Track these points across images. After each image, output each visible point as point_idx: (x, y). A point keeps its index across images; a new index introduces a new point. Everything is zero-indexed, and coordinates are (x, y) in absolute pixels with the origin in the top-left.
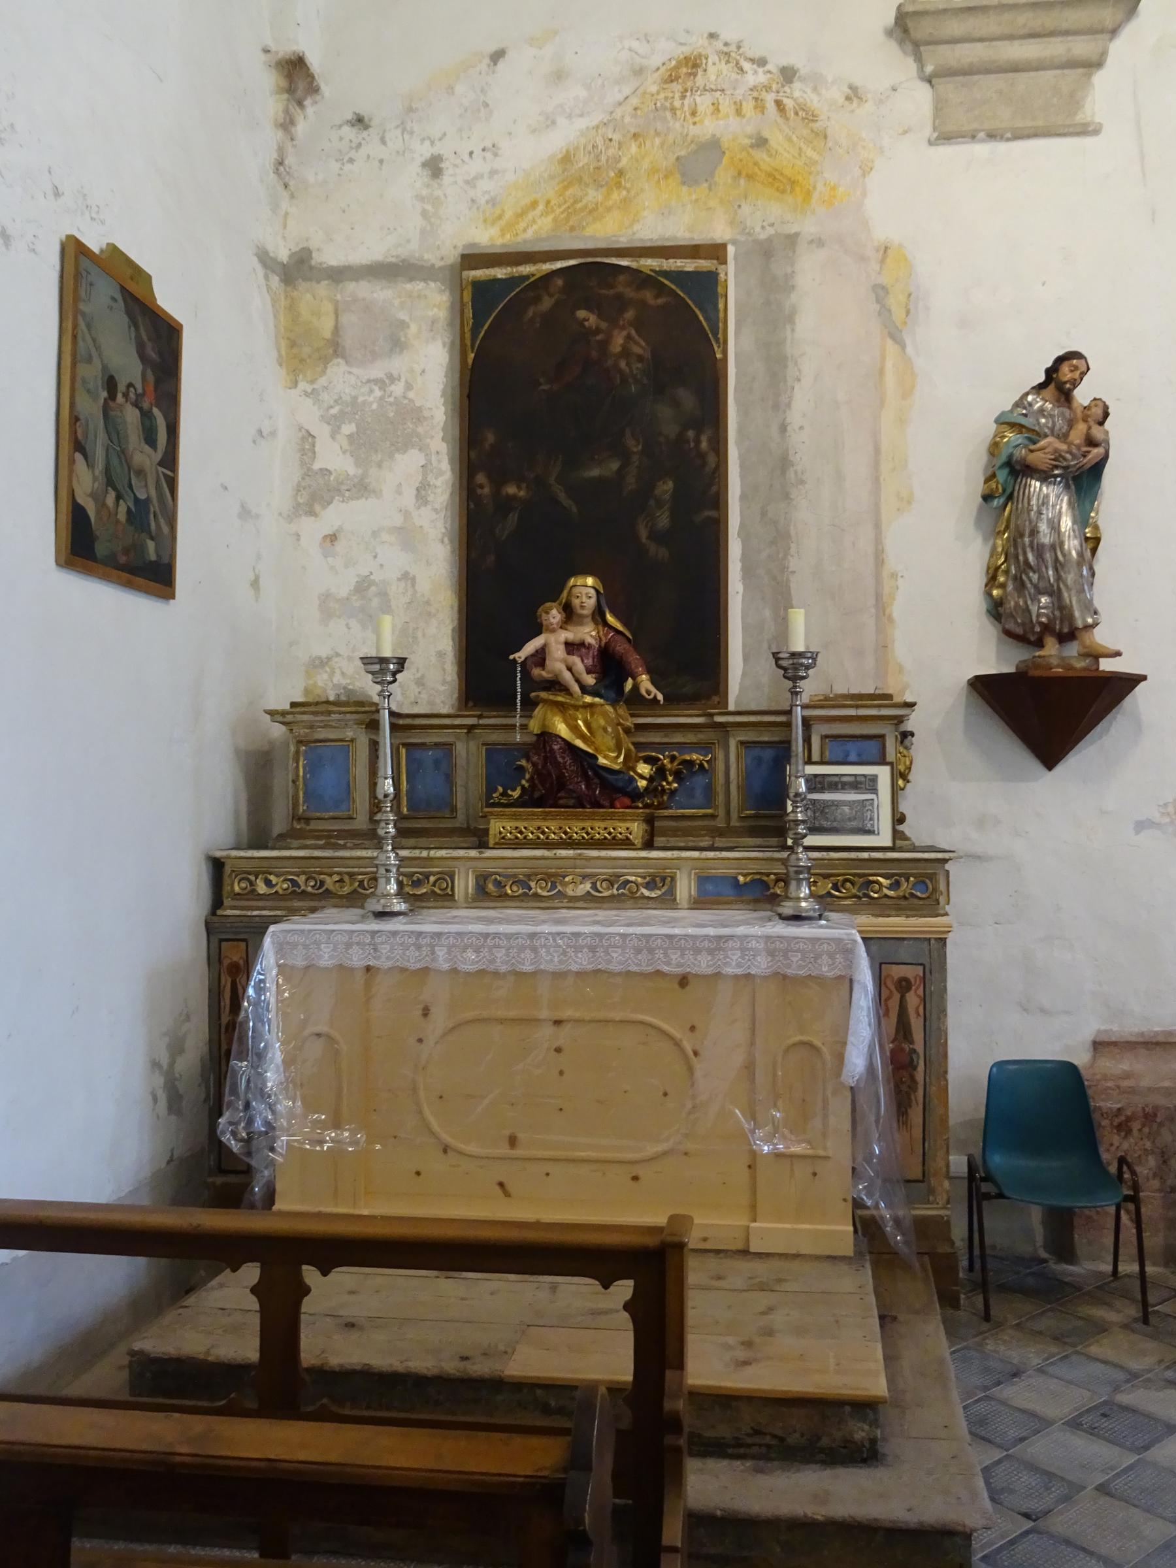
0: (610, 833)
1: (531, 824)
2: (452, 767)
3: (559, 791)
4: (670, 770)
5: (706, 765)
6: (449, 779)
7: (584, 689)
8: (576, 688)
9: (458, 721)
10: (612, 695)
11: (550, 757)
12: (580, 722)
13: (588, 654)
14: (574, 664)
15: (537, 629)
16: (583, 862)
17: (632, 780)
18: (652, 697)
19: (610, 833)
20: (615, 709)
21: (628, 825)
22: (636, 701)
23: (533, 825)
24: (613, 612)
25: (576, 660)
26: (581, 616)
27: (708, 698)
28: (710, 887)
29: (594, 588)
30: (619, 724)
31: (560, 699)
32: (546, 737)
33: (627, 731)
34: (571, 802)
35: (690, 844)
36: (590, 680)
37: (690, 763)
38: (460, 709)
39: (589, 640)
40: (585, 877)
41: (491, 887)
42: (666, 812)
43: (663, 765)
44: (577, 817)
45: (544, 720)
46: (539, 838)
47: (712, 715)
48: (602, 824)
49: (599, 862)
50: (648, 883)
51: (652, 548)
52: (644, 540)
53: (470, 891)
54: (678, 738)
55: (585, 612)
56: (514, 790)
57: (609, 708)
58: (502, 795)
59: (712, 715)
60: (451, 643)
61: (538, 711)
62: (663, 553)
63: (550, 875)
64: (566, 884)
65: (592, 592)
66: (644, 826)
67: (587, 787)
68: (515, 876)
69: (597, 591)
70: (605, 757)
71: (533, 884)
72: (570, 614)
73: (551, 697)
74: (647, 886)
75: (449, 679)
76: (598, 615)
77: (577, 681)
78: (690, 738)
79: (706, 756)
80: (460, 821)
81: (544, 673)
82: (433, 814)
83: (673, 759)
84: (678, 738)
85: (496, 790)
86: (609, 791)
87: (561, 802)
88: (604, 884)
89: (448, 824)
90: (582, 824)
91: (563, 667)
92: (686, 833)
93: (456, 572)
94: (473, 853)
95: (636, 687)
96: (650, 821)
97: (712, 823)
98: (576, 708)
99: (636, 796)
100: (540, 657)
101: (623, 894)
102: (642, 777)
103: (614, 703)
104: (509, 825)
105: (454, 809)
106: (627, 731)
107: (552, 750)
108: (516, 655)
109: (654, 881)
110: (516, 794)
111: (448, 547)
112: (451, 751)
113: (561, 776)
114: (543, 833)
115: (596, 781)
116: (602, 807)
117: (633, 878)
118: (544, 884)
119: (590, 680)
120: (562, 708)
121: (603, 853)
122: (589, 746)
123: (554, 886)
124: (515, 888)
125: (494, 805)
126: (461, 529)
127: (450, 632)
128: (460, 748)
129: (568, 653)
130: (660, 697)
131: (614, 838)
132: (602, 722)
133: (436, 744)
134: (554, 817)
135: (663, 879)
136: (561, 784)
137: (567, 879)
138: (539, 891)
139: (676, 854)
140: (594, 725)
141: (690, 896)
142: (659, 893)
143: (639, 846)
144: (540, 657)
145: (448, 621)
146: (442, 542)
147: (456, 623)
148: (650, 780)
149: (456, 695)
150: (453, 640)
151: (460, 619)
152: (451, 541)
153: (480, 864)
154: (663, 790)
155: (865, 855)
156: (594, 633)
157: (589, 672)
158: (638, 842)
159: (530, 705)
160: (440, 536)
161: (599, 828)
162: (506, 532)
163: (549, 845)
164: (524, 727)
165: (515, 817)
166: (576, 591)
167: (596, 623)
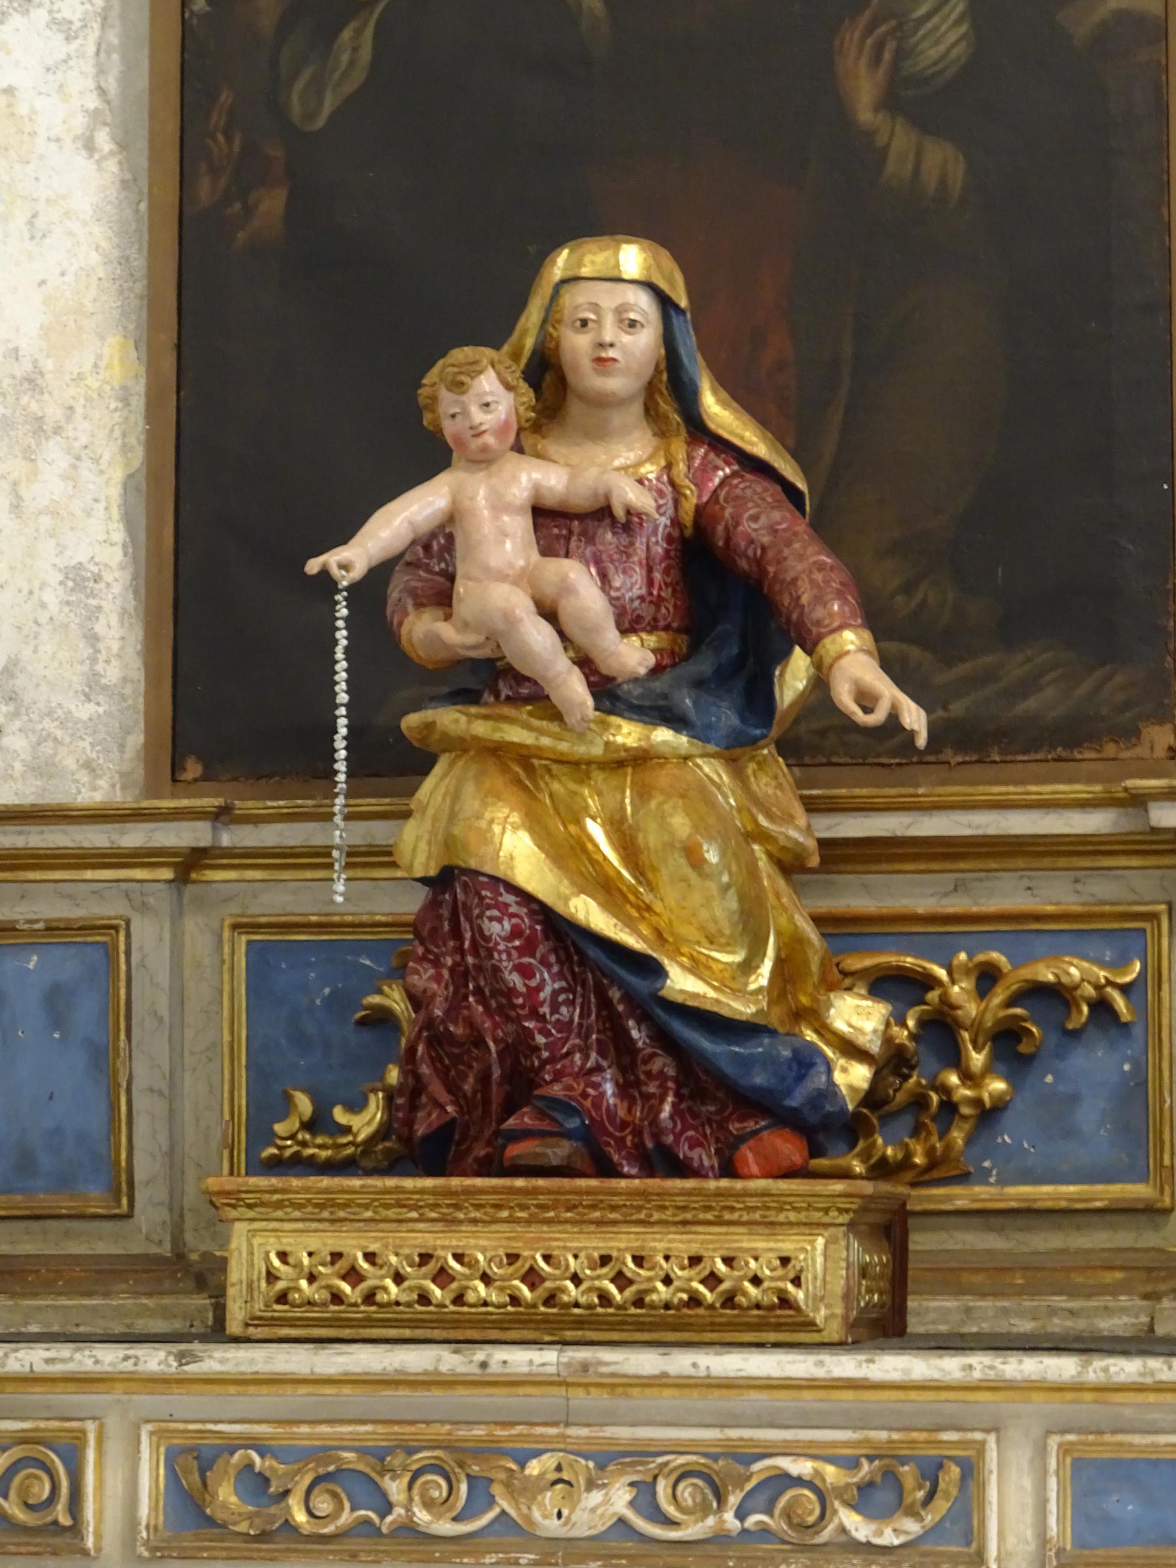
0: (712, 1280)
1: (403, 1235)
2: (118, 1016)
3: (510, 1108)
4: (976, 1027)
5: (1120, 1002)
6: (105, 1062)
7: (608, 693)
8: (574, 689)
9: (134, 837)
10: (727, 717)
11: (473, 975)
12: (595, 830)
13: (626, 552)
14: (567, 588)
15: (429, 455)
16: (600, 1399)
17: (805, 1061)
18: (878, 717)
19: (712, 1280)
20: (738, 774)
21: (787, 1245)
22: (825, 745)
23: (399, 1245)
24: (739, 392)
25: (582, 587)
26: (603, 402)
27: (1129, 734)
28: (1125, 1507)
29: (649, 285)
30: (758, 835)
31: (516, 735)
32: (457, 888)
33: (790, 865)
34: (559, 1151)
35: (1058, 1325)
36: (633, 655)
37: (1055, 996)
38: (151, 791)
39: (631, 495)
40: (607, 1460)
41: (227, 1495)
42: (961, 1197)
43: (946, 1002)
44: (582, 1215)
45: (453, 817)
46: (424, 1299)
47: (1138, 801)
48: (682, 1244)
49: (667, 1399)
50: (866, 1488)
51: (900, 141)
52: (865, 111)
53: (144, 1511)
54: (1006, 893)
55: (614, 384)
56: (356, 1106)
57: (711, 769)
58: (309, 1126)
59: (1138, 801)
60: (119, 535)
61: (432, 789)
62: (941, 163)
63: (463, 1452)
64: (530, 1490)
65: (643, 302)
66: (856, 1251)
67: (623, 1090)
68: (323, 1453)
69: (664, 302)
70: (697, 967)
71: (395, 1488)
72: (552, 394)
73: (481, 729)
74: (863, 1498)
75: (112, 673)
76: (669, 395)
77: (584, 662)
78: (1054, 893)
79: (1121, 963)
80: (147, 1229)
81: (448, 632)
82: (45, 1201)
83: (987, 978)
84: (1006, 893)
85: (286, 1107)
86: (714, 1102)
87: (515, 1150)
88: (686, 1491)
89: (102, 1243)
90: (596, 1244)
91: (521, 604)
92: (1041, 1277)
93: (139, 262)
94: (155, 1360)
95: (820, 683)
96: (889, 1229)
97: (1150, 1239)
98: (580, 768)
99: (825, 1130)
100: (435, 561)
101: (764, 1532)
102: (851, 1050)
103: (734, 750)
104: (308, 1243)
105: (122, 1185)
106: (790, 865)
107: (480, 936)
108: (332, 559)
109: (891, 1477)
110: (365, 1122)
111: (112, 166)
112: (109, 952)
113: (518, 1049)
114: (442, 1276)
115: (662, 1063)
116: (682, 1169)
117: (802, 1467)
118: (439, 1491)
119: (633, 655)
120: (522, 769)
121: (682, 1362)
122: (629, 923)
123: (480, 1489)
124: (323, 1505)
125: (276, 1166)
126: (155, 88)
127: (115, 492)
128: (148, 938)
129: (547, 551)
130: (914, 718)
131: (729, 1300)
132: (681, 824)
133: (52, 928)
134: (491, 1212)
135: (931, 1472)
136: (522, 1084)
137: (534, 1468)
138: (422, 1516)
139: (981, 1364)
140: (650, 838)
141: (1043, 1539)
142: (912, 1527)
143: (834, 1331)
144: (435, 561)
145: (108, 452)
146: (89, 146)
147: (138, 456)
148: (892, 1062)
149: (137, 740)
150: (128, 521)
151: (152, 443)
152: (123, 145)
153: (185, 1406)
154: (949, 1108)
155: (407, 1333)
156: (650, 471)
157: (628, 624)
158: (828, 1316)
159: (391, 764)
160: (79, 123)
161: (667, 1252)
162: (329, 103)
163: (465, 1327)
164: (371, 858)
165: (328, 1211)
166: (577, 299)
167: (662, 432)
